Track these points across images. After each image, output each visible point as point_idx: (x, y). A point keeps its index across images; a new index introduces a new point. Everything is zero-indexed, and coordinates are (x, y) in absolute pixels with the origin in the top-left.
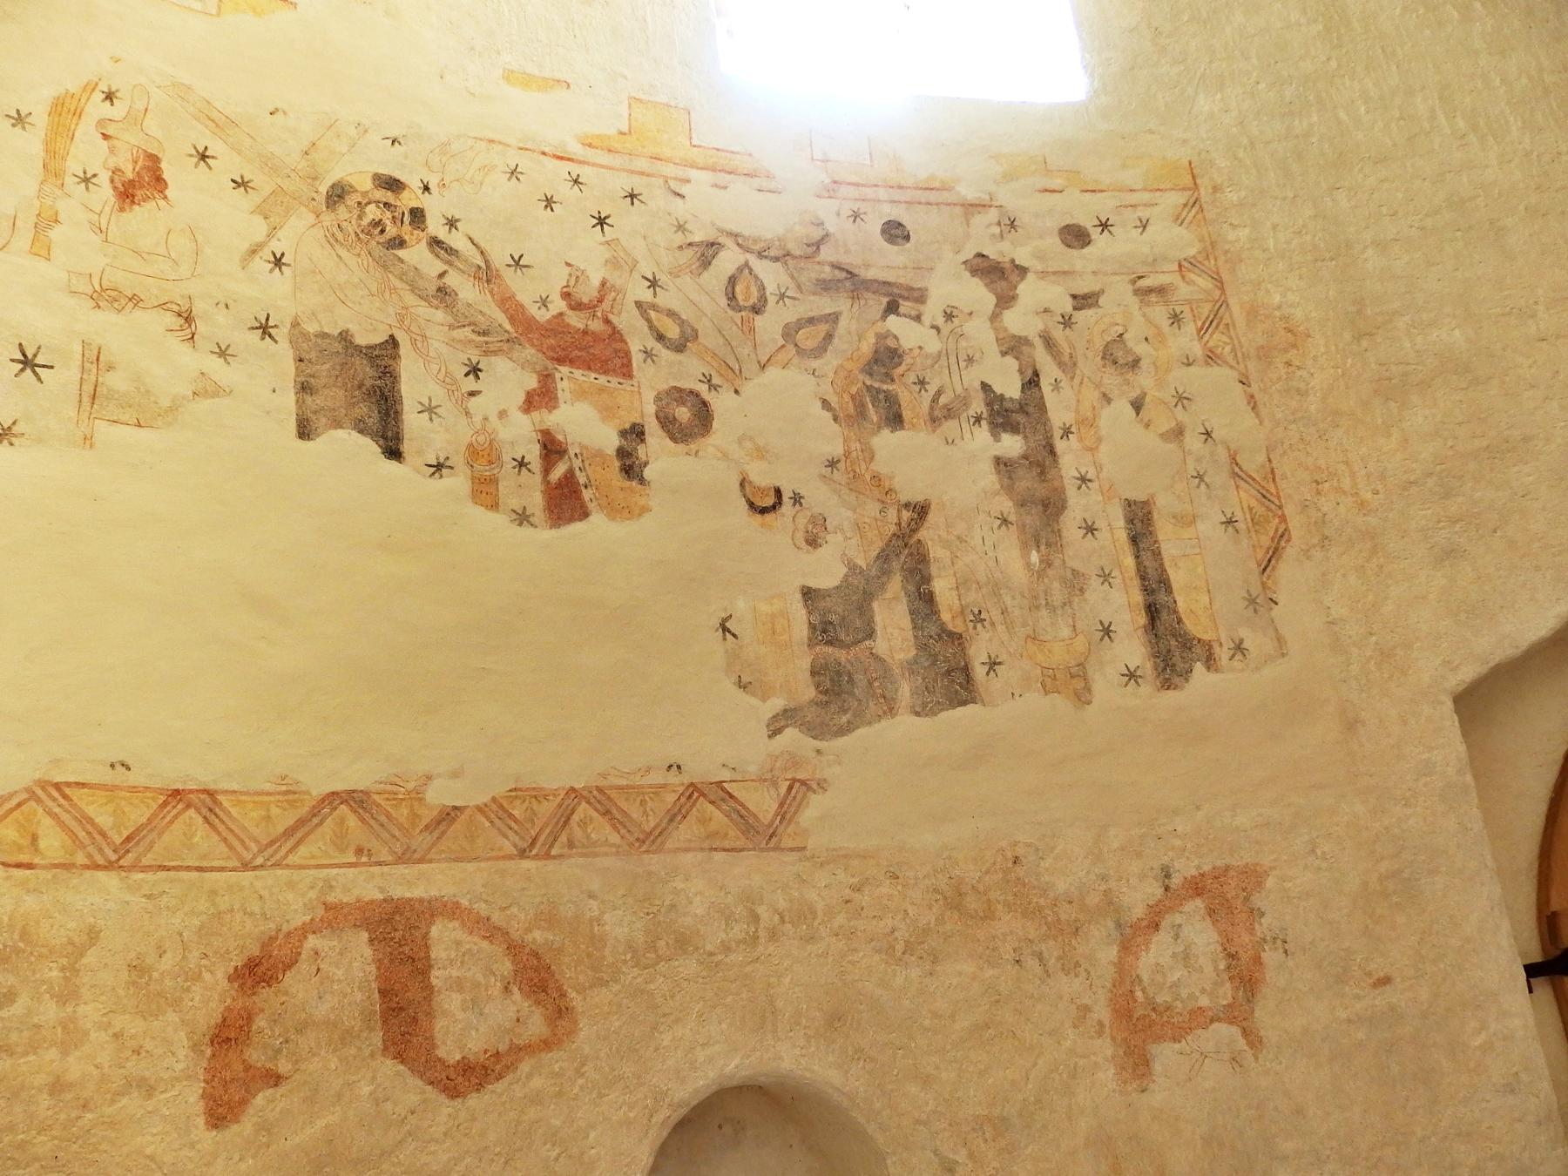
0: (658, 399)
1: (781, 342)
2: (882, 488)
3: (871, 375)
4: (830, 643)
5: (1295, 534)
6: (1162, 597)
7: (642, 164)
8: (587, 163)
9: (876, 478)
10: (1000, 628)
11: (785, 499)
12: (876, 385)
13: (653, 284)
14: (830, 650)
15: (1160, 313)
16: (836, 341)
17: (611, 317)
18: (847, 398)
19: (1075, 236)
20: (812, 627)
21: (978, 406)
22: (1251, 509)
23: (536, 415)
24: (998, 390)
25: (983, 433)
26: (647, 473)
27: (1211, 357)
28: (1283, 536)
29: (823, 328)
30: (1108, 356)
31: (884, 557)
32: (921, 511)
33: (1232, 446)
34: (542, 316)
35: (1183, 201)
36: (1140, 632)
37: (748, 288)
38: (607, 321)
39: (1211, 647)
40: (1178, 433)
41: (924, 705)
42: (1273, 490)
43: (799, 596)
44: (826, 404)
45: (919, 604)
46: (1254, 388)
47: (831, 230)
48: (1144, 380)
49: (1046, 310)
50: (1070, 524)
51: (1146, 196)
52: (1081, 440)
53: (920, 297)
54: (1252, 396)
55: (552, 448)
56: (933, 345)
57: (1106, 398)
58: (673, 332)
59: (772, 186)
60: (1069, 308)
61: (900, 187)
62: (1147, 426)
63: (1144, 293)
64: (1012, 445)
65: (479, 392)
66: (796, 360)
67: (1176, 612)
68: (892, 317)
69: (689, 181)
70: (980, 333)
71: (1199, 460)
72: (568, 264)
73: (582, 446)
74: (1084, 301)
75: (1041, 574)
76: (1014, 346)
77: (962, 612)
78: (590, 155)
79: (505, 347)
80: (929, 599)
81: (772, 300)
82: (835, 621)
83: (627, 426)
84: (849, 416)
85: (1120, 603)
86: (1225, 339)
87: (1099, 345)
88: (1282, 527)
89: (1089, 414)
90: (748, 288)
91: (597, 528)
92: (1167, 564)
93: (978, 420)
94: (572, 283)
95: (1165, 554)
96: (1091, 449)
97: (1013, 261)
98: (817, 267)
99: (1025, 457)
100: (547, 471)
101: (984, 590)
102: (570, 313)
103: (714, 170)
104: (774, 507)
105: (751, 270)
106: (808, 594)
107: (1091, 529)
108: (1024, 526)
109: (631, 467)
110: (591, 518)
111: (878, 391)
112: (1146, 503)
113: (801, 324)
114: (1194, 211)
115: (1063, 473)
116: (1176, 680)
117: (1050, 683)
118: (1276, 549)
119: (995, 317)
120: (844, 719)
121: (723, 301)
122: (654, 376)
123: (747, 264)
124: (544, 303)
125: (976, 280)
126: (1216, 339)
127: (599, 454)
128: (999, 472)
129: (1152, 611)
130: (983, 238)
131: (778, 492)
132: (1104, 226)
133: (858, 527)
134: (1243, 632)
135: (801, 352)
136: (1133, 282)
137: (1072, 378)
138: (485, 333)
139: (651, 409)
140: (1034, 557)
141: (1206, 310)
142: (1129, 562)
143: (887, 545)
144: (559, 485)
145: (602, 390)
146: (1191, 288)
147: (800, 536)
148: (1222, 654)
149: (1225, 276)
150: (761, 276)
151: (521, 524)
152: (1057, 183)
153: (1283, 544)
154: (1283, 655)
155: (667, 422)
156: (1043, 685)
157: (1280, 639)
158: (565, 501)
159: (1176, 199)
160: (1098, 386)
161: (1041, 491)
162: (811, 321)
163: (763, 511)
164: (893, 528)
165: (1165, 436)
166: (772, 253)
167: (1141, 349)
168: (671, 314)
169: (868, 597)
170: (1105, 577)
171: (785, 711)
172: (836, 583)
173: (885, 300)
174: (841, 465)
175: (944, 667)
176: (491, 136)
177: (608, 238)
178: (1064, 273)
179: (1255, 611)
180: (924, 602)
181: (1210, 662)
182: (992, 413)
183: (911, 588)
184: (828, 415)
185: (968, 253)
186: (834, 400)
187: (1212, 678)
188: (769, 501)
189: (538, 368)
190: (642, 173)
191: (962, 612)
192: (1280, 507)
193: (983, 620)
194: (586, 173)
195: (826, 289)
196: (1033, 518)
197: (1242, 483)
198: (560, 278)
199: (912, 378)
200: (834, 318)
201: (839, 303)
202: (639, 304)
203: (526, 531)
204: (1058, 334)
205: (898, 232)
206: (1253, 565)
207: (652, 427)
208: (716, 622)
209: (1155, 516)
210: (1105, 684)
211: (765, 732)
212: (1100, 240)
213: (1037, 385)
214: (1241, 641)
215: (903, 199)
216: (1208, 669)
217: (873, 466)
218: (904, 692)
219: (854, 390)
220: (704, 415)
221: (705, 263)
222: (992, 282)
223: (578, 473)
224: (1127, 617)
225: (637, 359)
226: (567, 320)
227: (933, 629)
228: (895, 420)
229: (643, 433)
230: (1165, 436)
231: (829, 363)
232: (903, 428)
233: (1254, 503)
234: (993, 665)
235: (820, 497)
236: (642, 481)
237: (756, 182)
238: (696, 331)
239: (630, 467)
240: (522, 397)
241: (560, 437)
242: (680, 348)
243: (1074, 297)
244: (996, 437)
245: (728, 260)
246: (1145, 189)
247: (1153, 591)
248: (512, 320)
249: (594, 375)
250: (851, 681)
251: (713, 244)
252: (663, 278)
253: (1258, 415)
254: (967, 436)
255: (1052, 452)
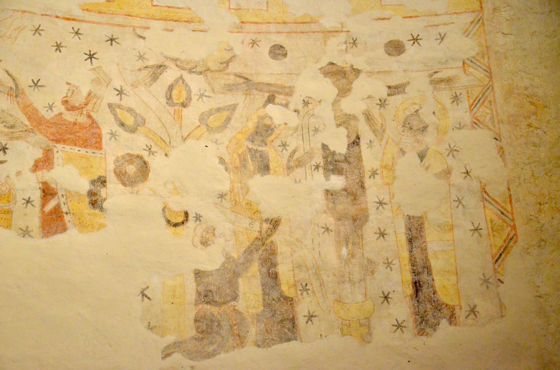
0: (117, 161)
1: (198, 123)
2: (253, 210)
3: (253, 141)
4: (208, 303)
5: (520, 238)
6: (424, 277)
7: (119, 20)
8: (85, 21)
9: (249, 204)
10: (319, 295)
11: (191, 217)
12: (255, 148)
13: (120, 92)
14: (208, 307)
15: (445, 96)
16: (232, 122)
17: (92, 114)
18: (235, 156)
19: (395, 48)
20: (199, 293)
21: (318, 159)
22: (492, 222)
23: (39, 173)
24: (332, 148)
25: (320, 175)
26: (105, 205)
27: (476, 123)
28: (512, 239)
29: (226, 114)
30: (407, 125)
31: (249, 251)
32: (275, 223)
33: (483, 181)
34: (48, 115)
35: (471, 19)
36: (408, 298)
37: (180, 92)
38: (89, 116)
39: (454, 309)
40: (448, 172)
41: (264, 341)
42: (509, 209)
43: (193, 275)
44: (222, 161)
45: (270, 281)
46: (504, 143)
47: (237, 53)
48: (429, 139)
49: (369, 97)
50: (369, 231)
51: (446, 18)
52: (382, 177)
53: (289, 92)
54: (501, 148)
55: (48, 192)
56: (294, 120)
57: (403, 152)
58: (130, 120)
59: (202, 27)
60: (385, 95)
61: (284, 23)
62: (427, 168)
63: (437, 83)
64: (337, 182)
65: (5, 161)
66: (206, 134)
67: (433, 286)
68: (270, 106)
69: (148, 28)
70: (326, 113)
71: (459, 190)
72: (68, 84)
73: (66, 190)
74: (395, 90)
75: (347, 262)
76: (345, 121)
77: (295, 285)
78: (87, 16)
79: (23, 134)
80: (275, 277)
81: (194, 98)
82: (212, 292)
83: (96, 178)
84: (236, 167)
85: (399, 281)
86: (488, 111)
87: (401, 118)
88: (513, 232)
89: (390, 163)
90: (180, 92)
91: (71, 238)
92: (430, 256)
93: (317, 167)
94: (70, 94)
95: (430, 251)
96: (388, 184)
97: (352, 66)
98: (226, 77)
99: (345, 190)
100: (43, 206)
101: (310, 272)
102: (67, 113)
103: (166, 20)
104: (183, 223)
105: (183, 80)
106: (198, 274)
107: (382, 234)
108: (339, 232)
109: (96, 201)
110: (68, 232)
111: (256, 151)
112: (421, 218)
113: (210, 113)
114: (477, 26)
115: (369, 200)
116: (428, 330)
117: (345, 329)
118: (506, 247)
119: (335, 103)
120: (211, 348)
121: (164, 100)
122: (116, 147)
123: (181, 77)
124: (51, 107)
125: (328, 80)
126: (483, 112)
127: (78, 194)
128: (327, 199)
129: (417, 286)
130: (334, 51)
131: (186, 214)
132: (415, 40)
133: (235, 233)
134: (477, 301)
135: (210, 129)
136: (431, 76)
137: (381, 140)
138: (12, 127)
139: (111, 167)
140: (344, 251)
141: (477, 91)
142: (405, 254)
143: (252, 244)
144: (51, 213)
145: (82, 157)
146: (471, 78)
147: (197, 240)
148: (461, 315)
149: (494, 69)
150: (190, 84)
151: (24, 236)
152: (388, 13)
153: (511, 244)
154: (502, 316)
155: (120, 175)
156: (342, 330)
157: (501, 306)
158: (53, 222)
159: (468, 18)
160: (397, 144)
161: (353, 210)
162: (218, 110)
163: (176, 225)
164: (256, 234)
165: (437, 175)
166: (198, 69)
167: (429, 119)
168: (130, 110)
169: (236, 275)
170: (388, 264)
171: (175, 343)
172: (217, 267)
173: (267, 95)
174: (228, 197)
175: (280, 318)
176: (24, 8)
177: (94, 66)
178: (385, 72)
179: (487, 287)
180: (272, 277)
181: (452, 319)
182: (326, 163)
183: (264, 270)
184: (222, 167)
185: (324, 63)
186: (227, 158)
187: (451, 329)
188: (180, 219)
189: (43, 146)
190: (119, 25)
191: (295, 285)
192: (513, 220)
193: (307, 290)
194: (84, 28)
195: (230, 90)
196: (346, 227)
197: (487, 204)
198: (62, 92)
199: (278, 142)
200: (233, 108)
201: (239, 99)
202: (110, 106)
203: (28, 241)
204: (376, 112)
205: (280, 52)
206: (489, 257)
207: (111, 178)
208: (138, 291)
209: (426, 226)
210: (382, 331)
211: (160, 355)
212: (411, 50)
213: (358, 144)
214: (475, 306)
215: (286, 30)
216: (450, 323)
217: (247, 197)
218: (253, 331)
219: (240, 151)
220: (144, 169)
221: (155, 78)
222: (338, 80)
223: (62, 206)
224: (399, 289)
225: (106, 137)
226: (64, 117)
227: (275, 295)
228: (265, 168)
229: (105, 182)
230: (437, 175)
231: (228, 133)
232: (269, 173)
233: (494, 218)
234: (310, 317)
235: (213, 215)
236: (101, 209)
237: (192, 26)
238: (144, 120)
239: (95, 201)
240: (32, 163)
241: (53, 186)
242: (133, 130)
243: (389, 87)
244: (327, 178)
245: (170, 75)
246: (446, 14)
247: (419, 274)
248: (29, 118)
249: (78, 149)
250: (219, 325)
251: (160, 66)
252: (127, 89)
253: (504, 160)
254: (309, 177)
255: (363, 187)
